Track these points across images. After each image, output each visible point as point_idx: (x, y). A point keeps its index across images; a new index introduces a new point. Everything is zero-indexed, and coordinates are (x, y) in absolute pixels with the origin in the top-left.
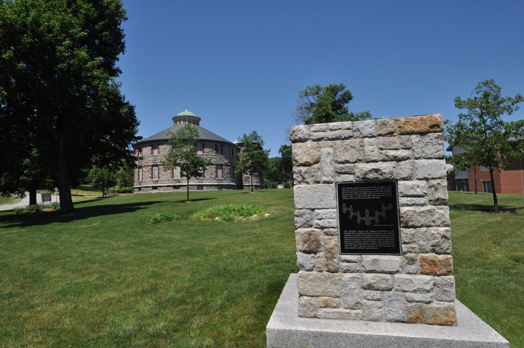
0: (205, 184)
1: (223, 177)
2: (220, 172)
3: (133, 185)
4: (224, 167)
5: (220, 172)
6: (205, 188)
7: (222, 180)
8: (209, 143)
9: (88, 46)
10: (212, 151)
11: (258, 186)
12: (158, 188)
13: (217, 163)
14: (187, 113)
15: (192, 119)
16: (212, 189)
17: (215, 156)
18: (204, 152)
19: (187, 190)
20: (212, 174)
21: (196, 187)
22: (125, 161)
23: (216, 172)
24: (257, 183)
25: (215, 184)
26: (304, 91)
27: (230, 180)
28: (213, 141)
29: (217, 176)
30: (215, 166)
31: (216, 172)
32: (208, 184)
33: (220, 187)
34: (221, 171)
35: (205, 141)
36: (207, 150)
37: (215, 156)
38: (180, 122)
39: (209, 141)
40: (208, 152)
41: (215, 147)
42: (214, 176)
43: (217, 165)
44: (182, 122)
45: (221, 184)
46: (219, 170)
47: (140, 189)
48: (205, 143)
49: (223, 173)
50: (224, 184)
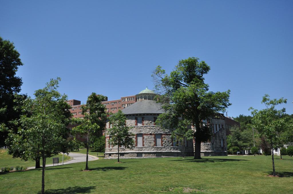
0: (144, 152)
1: (162, 145)
2: (159, 141)
3: (104, 152)
4: (163, 136)
5: (159, 141)
6: (143, 155)
7: (162, 148)
8: (148, 116)
9: (11, 65)
10: (151, 123)
11: (209, 153)
12: (112, 155)
13: (156, 133)
14: (146, 91)
15: (147, 96)
16: (151, 156)
17: (153, 127)
18: (143, 125)
19: (118, 158)
20: (150, 143)
21: (136, 154)
22: (284, 114)
23: (155, 141)
24: (207, 150)
25: (153, 151)
26: (171, 79)
27: (171, 148)
28: (151, 114)
29: (156, 144)
30: (154, 136)
31: (155, 141)
32: (146, 151)
33: (159, 154)
34: (161, 139)
35: (144, 114)
36: (146, 122)
37: (153, 127)
38: (142, 98)
39: (148, 114)
40: (147, 124)
41: (153, 119)
42: (152, 145)
43: (155, 135)
44: (140, 99)
45: (160, 151)
46: (158, 139)
47: (110, 155)
48: (144, 116)
49: (162, 141)
50: (163, 151)
